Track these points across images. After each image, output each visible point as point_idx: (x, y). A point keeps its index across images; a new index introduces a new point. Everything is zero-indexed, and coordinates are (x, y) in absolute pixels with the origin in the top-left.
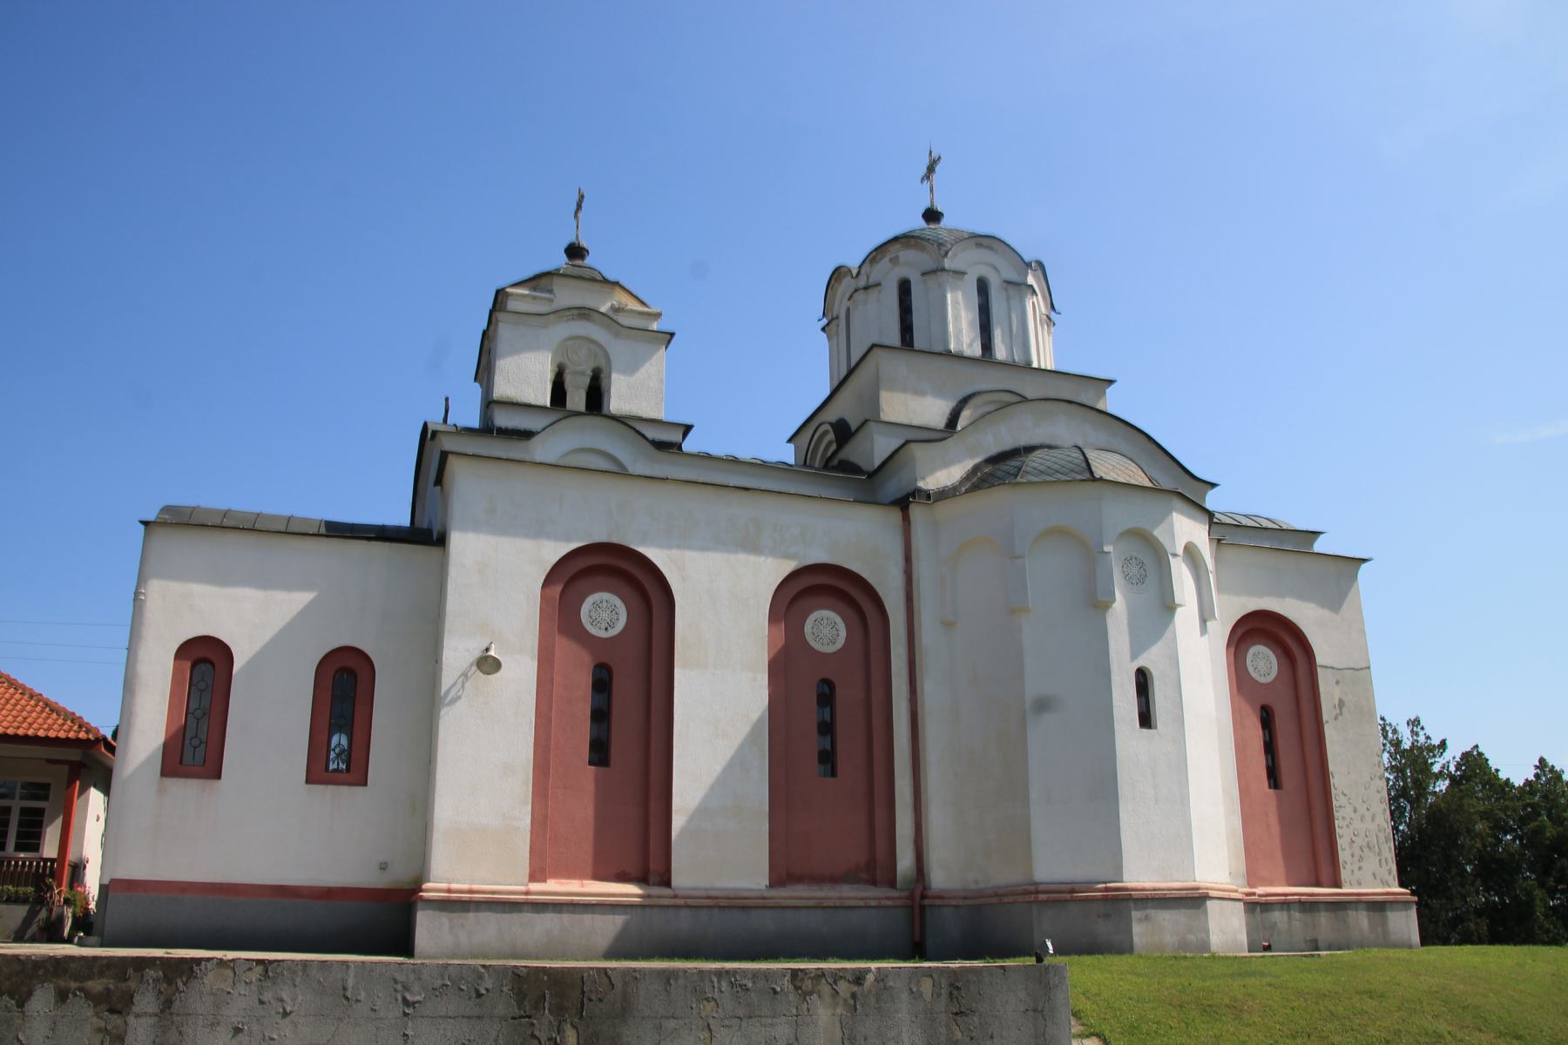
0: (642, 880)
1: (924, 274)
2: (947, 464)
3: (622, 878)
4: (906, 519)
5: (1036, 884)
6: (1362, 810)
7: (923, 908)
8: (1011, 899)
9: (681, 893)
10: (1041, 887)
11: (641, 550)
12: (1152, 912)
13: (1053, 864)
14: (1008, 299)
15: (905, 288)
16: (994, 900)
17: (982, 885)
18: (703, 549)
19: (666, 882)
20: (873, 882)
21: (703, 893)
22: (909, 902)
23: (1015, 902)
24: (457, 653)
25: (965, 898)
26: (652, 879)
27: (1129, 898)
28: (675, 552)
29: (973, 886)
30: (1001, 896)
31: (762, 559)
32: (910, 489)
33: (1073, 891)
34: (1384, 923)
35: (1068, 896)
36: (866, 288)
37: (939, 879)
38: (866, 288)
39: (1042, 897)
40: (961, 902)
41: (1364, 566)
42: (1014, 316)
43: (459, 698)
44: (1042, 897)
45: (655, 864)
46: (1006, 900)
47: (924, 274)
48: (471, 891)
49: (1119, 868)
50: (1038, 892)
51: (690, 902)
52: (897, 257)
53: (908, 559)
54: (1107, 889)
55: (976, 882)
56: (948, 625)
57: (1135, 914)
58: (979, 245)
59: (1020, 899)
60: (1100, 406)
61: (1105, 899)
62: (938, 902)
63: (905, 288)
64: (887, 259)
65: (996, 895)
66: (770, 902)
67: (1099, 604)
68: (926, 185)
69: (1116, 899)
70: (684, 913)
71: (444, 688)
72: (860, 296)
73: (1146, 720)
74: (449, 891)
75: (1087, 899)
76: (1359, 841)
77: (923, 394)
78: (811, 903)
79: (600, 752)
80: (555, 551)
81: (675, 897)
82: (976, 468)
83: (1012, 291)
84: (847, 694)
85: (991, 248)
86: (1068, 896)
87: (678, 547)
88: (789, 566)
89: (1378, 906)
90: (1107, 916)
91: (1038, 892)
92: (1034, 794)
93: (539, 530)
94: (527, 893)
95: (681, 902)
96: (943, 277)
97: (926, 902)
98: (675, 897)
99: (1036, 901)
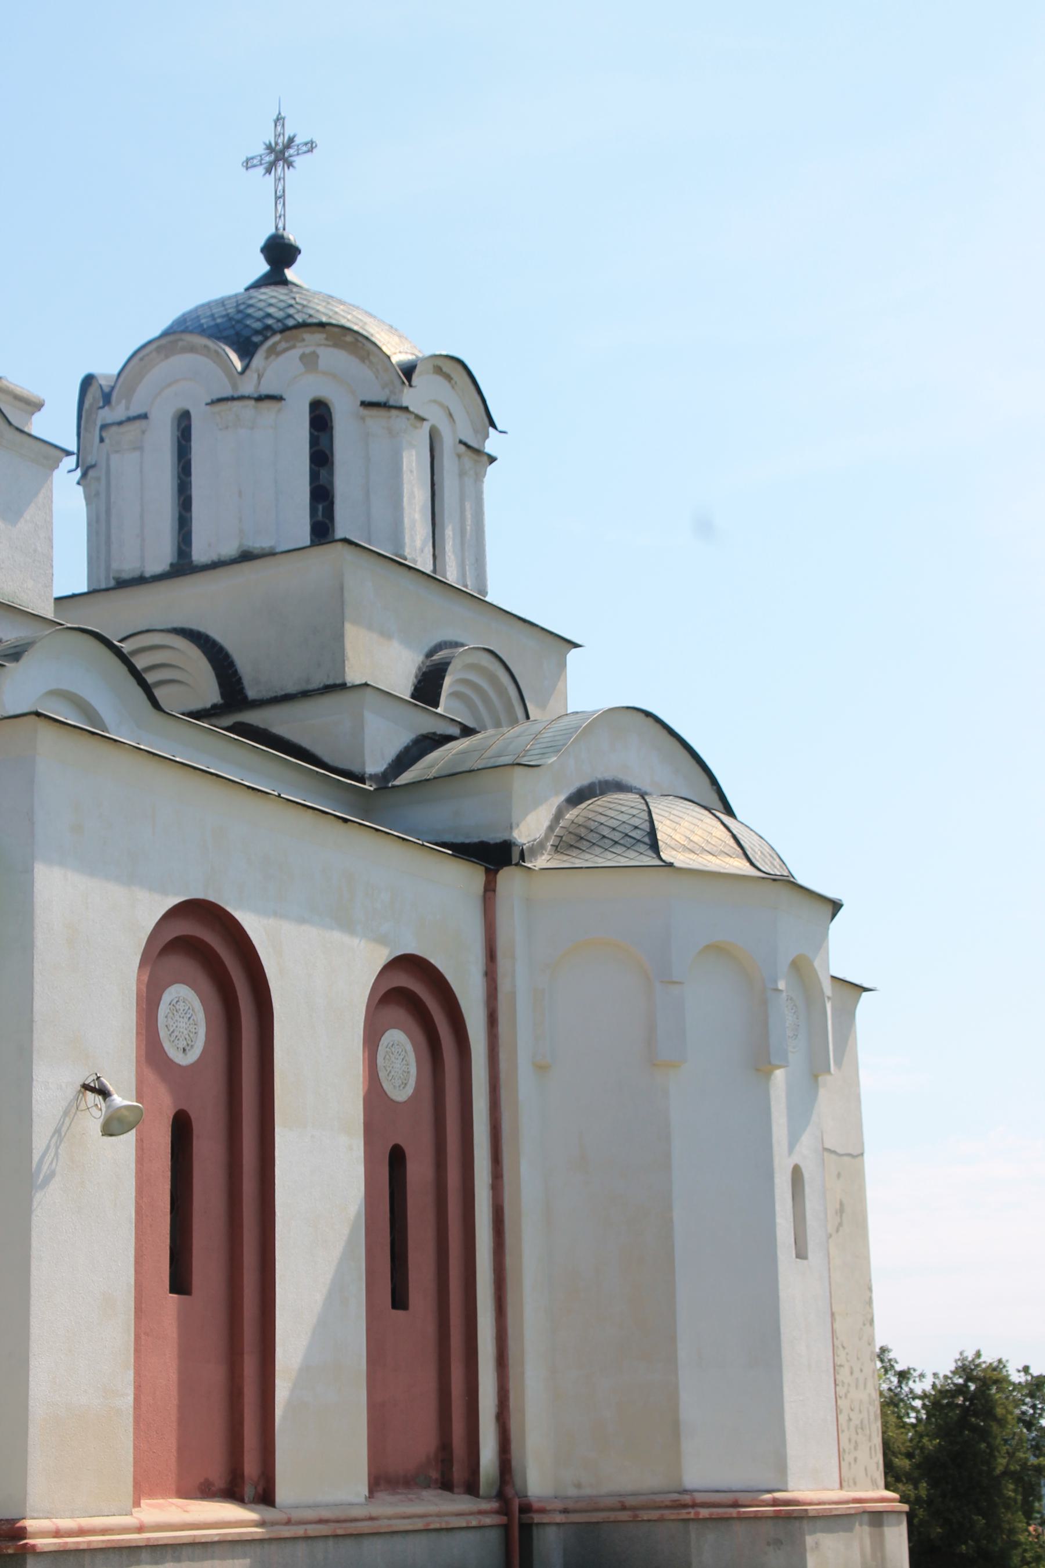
0: (232, 1493)
1: (365, 404)
2: (537, 803)
3: (206, 1492)
4: (490, 888)
5: (685, 1491)
6: (856, 1370)
7: (527, 1529)
8: (654, 1514)
9: (296, 1515)
10: (700, 1498)
11: (238, 915)
12: (820, 1536)
13: (706, 1467)
14: (462, 474)
15: (321, 418)
16: (624, 1516)
17: (587, 1491)
18: (302, 920)
19: (266, 1497)
20: (446, 1485)
21: (310, 1514)
22: (504, 1519)
23: (661, 1520)
24: (52, 1085)
25: (565, 1511)
26: (249, 1491)
27: (803, 1517)
28: (272, 922)
29: (572, 1492)
30: (631, 1510)
31: (356, 941)
32: (494, 837)
33: (736, 1505)
34: (882, 1536)
35: (733, 1512)
36: (260, 399)
37: (538, 1480)
38: (260, 399)
39: (704, 1512)
40: (559, 1518)
41: (864, 994)
42: (468, 506)
43: (52, 1175)
44: (704, 1512)
45: (251, 1467)
46: (645, 1515)
47: (365, 404)
48: (81, 1532)
49: (781, 1466)
50: (694, 1505)
51: (313, 1530)
52: (315, 355)
53: (491, 954)
54: (775, 1503)
55: (579, 1486)
56: (541, 1068)
57: (809, 1540)
58: (438, 370)
59: (669, 1514)
60: (26, 430)
61: (777, 1517)
62: (545, 1519)
63: (321, 418)
64: (296, 353)
65: (624, 1508)
66: (383, 1525)
67: (761, 1062)
68: (262, 183)
69: (790, 1517)
70: (301, 1549)
71: (34, 1165)
72: (247, 410)
73: (801, 1254)
74: (57, 1534)
75: (757, 1518)
76: (856, 1421)
77: (386, 634)
78: (419, 1524)
79: (180, 1282)
80: (150, 909)
81: (289, 1522)
82: (558, 816)
83: (468, 459)
84: (419, 1172)
85: (448, 378)
86: (733, 1512)
87: (276, 914)
88: (383, 956)
89: (877, 1518)
90: (778, 1543)
91: (694, 1505)
92: (683, 1354)
93: (131, 873)
94: (141, 1529)
95: (300, 1531)
96: (399, 420)
97: (537, 1518)
98: (289, 1522)
99: (697, 1520)
